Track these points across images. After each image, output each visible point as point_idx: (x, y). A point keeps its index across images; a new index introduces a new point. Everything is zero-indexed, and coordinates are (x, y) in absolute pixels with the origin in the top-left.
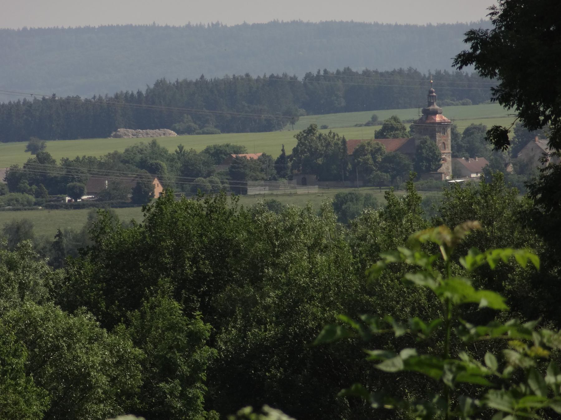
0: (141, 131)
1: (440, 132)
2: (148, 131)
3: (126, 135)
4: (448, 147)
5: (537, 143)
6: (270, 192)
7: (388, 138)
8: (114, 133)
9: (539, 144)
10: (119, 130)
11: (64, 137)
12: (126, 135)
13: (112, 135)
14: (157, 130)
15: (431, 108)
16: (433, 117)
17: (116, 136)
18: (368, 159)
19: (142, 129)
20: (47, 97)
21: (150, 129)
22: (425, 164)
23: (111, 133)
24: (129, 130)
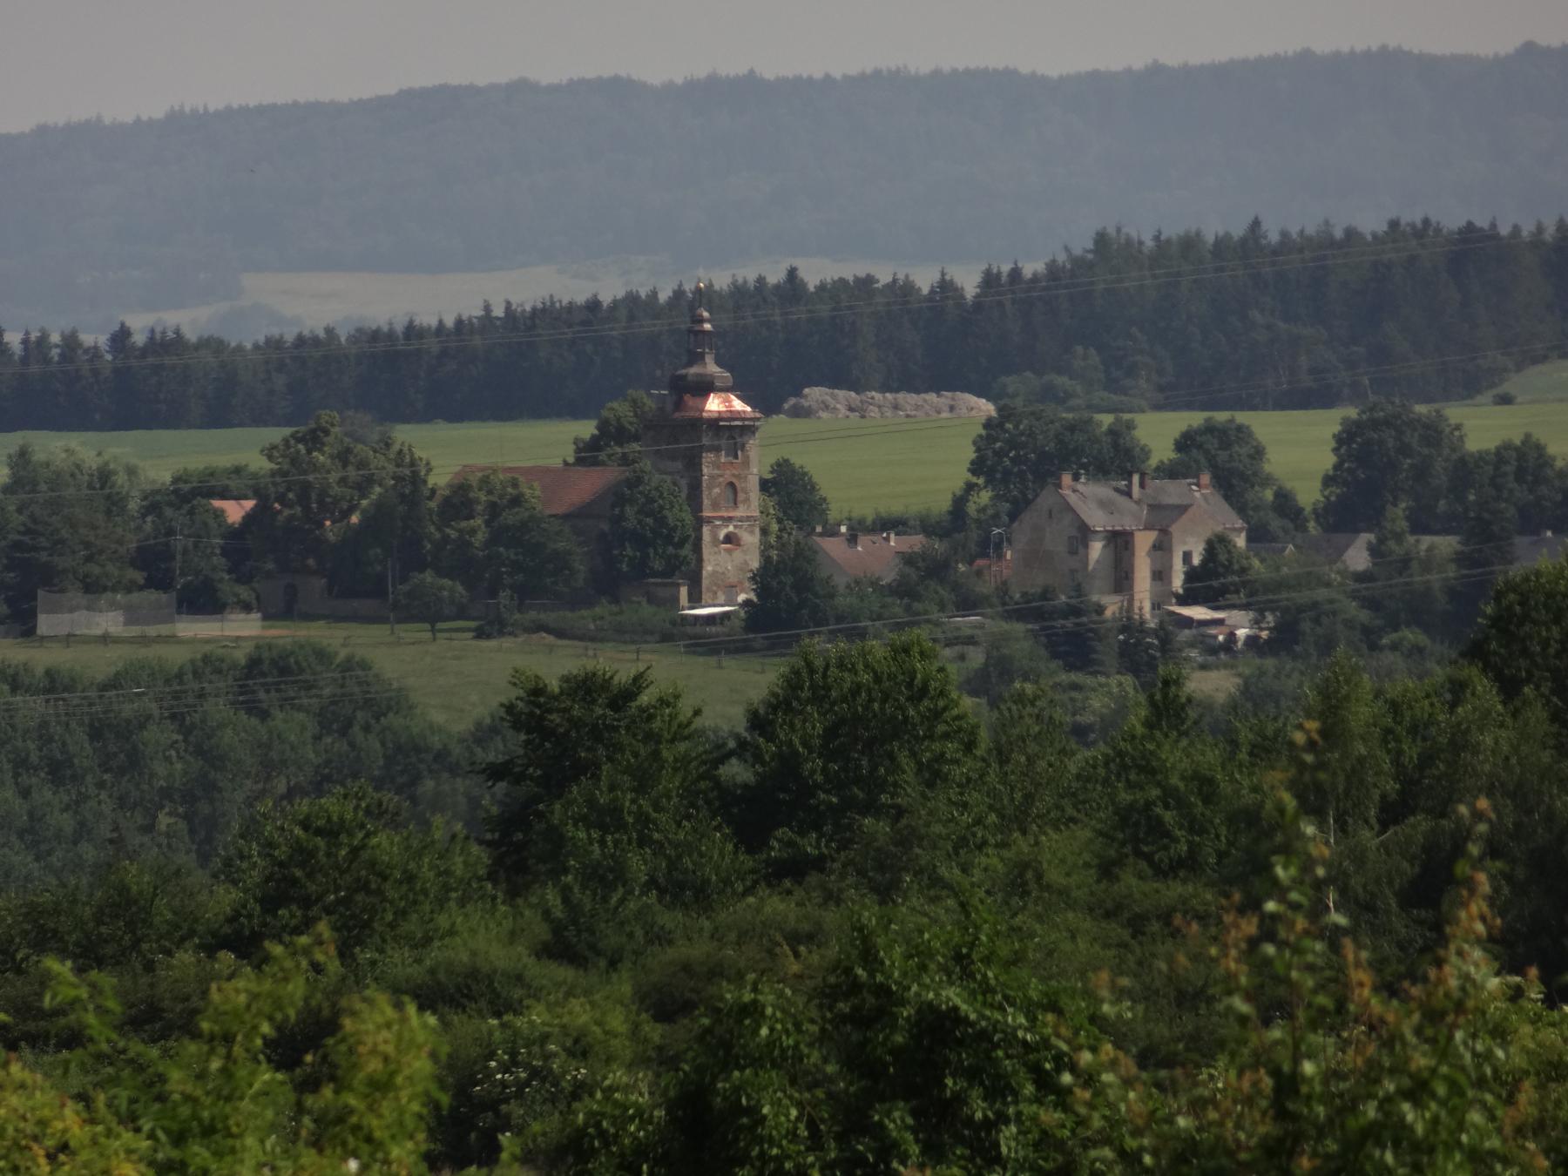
0: (877, 396)
1: (717, 449)
2: (901, 396)
3: (826, 407)
4: (747, 500)
5: (1066, 492)
6: (135, 631)
7: (603, 464)
8: (792, 401)
9: (1073, 499)
10: (807, 391)
11: (457, 414)
12: (826, 407)
13: (786, 406)
14: (931, 397)
15: (693, 370)
16: (698, 401)
17: (799, 413)
18: (473, 531)
19: (938, 391)
20: (1380, 233)
21: (909, 391)
22: (629, 552)
23: (784, 400)
24: (841, 393)
